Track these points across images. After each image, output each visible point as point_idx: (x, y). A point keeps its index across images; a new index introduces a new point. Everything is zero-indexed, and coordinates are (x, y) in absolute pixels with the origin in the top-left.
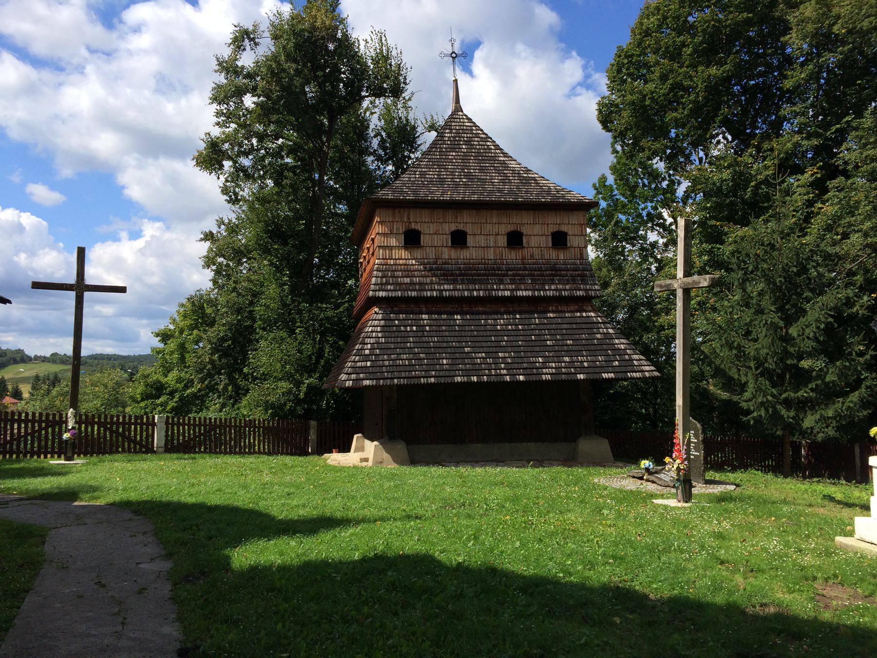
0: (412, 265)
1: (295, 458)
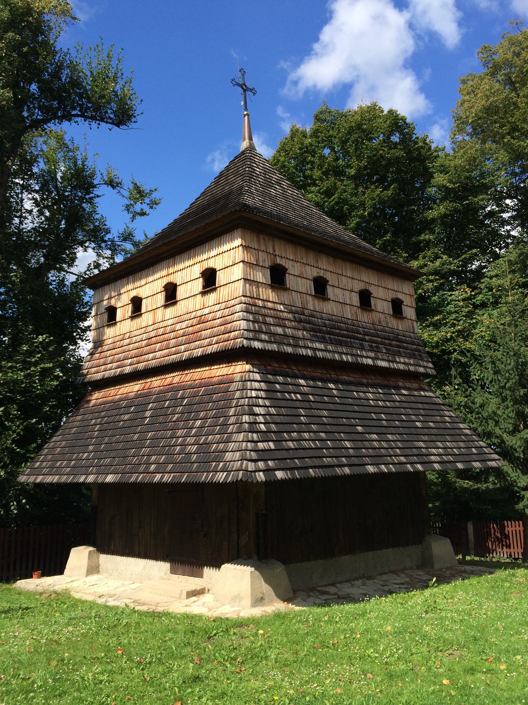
0: (281, 311)
1: (400, 597)
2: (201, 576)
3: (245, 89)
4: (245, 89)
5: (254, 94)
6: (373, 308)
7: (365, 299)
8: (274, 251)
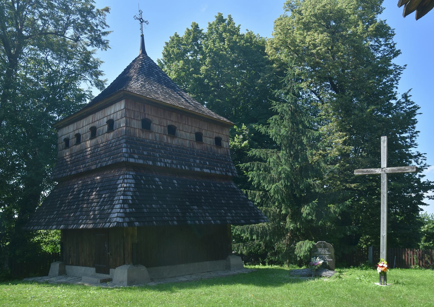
2: (109, 273)
3: (142, 21)
4: (142, 21)
5: (147, 24)
6: (204, 141)
7: (199, 137)
8: (144, 111)
